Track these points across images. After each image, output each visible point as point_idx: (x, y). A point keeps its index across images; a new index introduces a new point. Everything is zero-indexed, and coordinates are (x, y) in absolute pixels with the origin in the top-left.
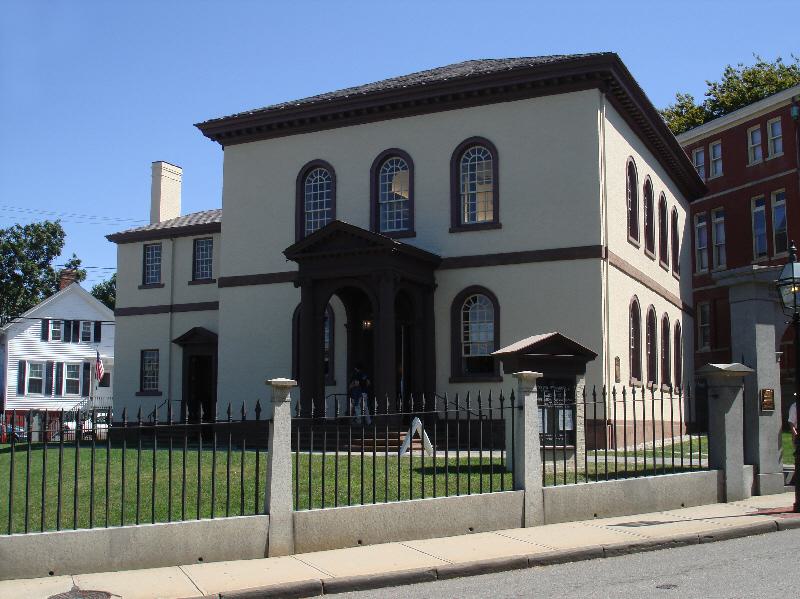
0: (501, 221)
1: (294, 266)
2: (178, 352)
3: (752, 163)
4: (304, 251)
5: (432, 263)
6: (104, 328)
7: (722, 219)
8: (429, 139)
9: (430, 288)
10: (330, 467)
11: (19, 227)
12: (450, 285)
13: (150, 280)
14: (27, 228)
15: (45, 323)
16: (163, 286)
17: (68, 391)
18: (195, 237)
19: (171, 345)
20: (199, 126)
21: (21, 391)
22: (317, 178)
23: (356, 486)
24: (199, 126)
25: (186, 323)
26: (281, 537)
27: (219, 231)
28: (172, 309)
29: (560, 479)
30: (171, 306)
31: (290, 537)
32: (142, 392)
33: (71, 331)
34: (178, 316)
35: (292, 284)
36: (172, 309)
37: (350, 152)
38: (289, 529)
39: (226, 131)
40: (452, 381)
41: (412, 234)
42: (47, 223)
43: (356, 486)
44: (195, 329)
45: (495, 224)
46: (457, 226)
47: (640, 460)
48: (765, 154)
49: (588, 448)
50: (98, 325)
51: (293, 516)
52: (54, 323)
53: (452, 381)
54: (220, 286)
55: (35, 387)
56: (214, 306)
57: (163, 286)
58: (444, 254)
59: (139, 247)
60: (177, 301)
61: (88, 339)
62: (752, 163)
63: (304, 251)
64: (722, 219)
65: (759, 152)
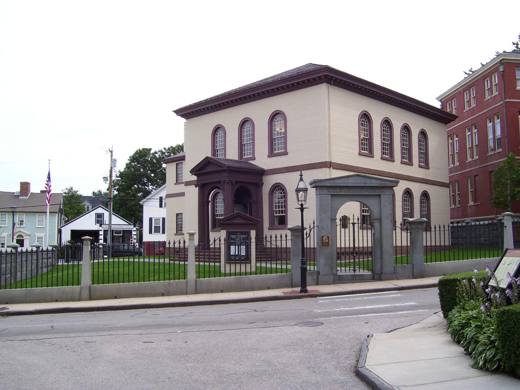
1: (195, 178)
4: (197, 171)
5: (261, 173)
8: (259, 111)
9: (259, 185)
10: (177, 268)
11: (165, 149)
12: (270, 181)
14: (169, 149)
17: (155, 232)
18: (177, 162)
20: (175, 112)
21: (150, 232)
24: (175, 112)
26: (85, 294)
27: (184, 159)
29: (212, 273)
31: (88, 294)
32: (177, 234)
38: (88, 291)
39: (188, 113)
40: (270, 229)
41: (254, 159)
47: (284, 267)
49: (256, 261)
51: (90, 287)
53: (270, 229)
54: (185, 185)
55: (157, 230)
56: (182, 194)
58: (266, 168)
63: (197, 171)
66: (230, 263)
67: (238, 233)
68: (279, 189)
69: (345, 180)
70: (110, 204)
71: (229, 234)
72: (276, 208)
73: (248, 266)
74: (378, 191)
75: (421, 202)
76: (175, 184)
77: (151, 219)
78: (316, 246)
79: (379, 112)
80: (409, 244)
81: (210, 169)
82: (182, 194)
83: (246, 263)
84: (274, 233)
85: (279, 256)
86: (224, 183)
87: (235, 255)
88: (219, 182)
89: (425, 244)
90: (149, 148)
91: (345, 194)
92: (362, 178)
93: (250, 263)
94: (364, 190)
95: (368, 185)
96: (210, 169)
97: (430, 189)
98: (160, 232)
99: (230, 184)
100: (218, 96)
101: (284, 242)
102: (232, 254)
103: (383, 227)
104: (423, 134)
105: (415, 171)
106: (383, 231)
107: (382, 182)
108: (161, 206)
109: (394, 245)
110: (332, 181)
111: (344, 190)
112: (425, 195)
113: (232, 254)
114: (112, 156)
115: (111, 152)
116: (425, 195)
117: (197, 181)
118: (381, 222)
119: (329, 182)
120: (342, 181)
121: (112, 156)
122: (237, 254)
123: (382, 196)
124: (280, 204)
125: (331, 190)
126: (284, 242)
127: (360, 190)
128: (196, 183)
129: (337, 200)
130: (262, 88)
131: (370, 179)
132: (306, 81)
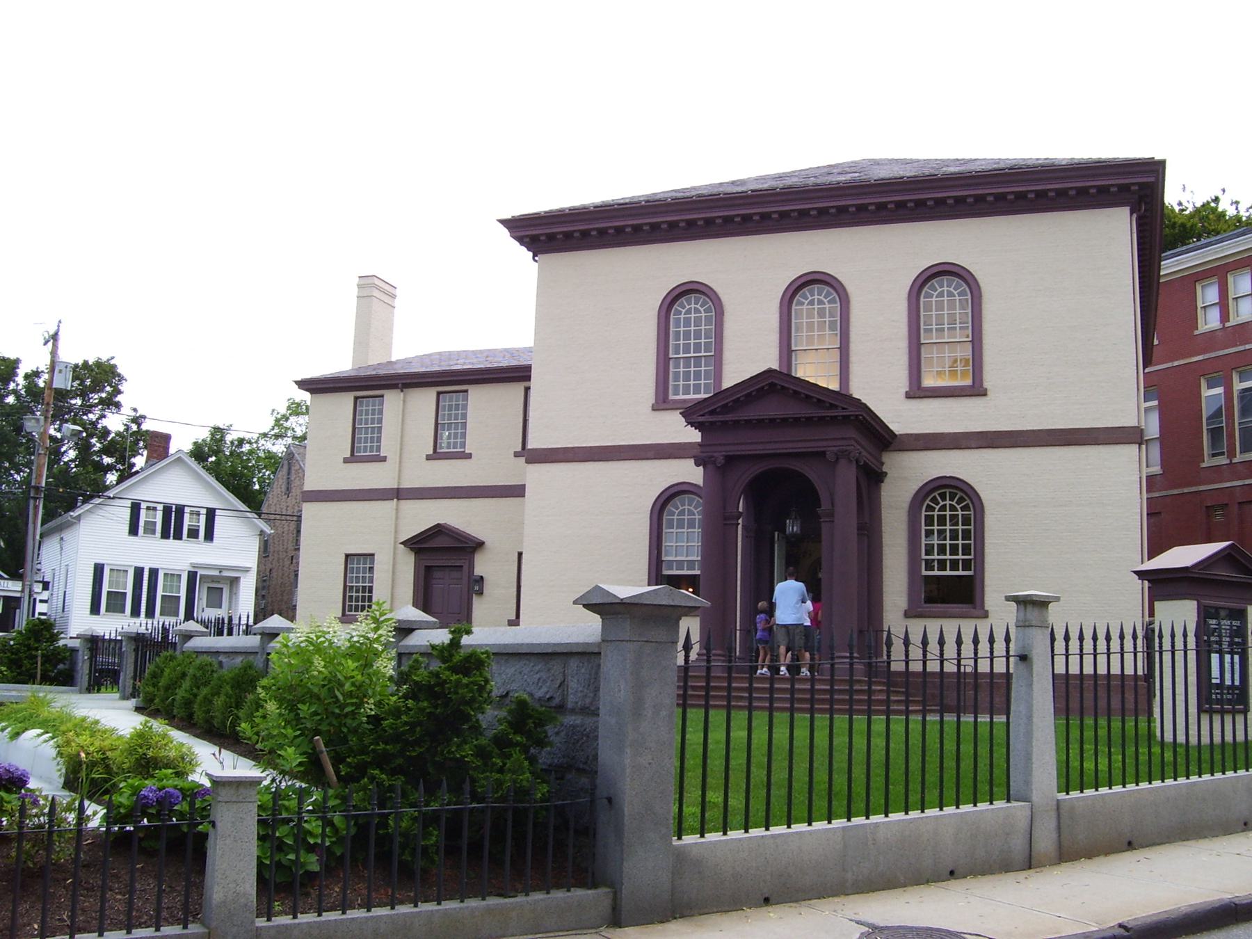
0: (986, 385)
1: (694, 436)
2: (407, 564)
3: (1202, 328)
6: (219, 521)
7: (1155, 403)
8: (877, 264)
9: (873, 477)
12: (908, 474)
13: (363, 450)
15: (135, 508)
16: (384, 459)
19: (395, 548)
20: (503, 222)
21: (95, 609)
22: (691, 308)
23: (736, 802)
25: (421, 517)
28: (399, 494)
30: (398, 489)
33: (173, 522)
34: (409, 506)
35: (692, 461)
36: (399, 494)
37: (753, 274)
39: (545, 234)
42: (86, 363)
43: (736, 802)
44: (438, 525)
45: (976, 390)
46: (917, 391)
48: (1225, 317)
50: (211, 514)
52: (192, 513)
56: (517, 491)
57: (384, 459)
59: (345, 402)
60: (406, 484)
61: (154, 532)
62: (1202, 328)
63: (712, 413)
64: (1155, 403)
65: (1214, 315)
66: (1211, 712)
70: (36, 507)
71: (1205, 614)
76: (346, 461)
77: (99, 570)
78: (1140, 672)
82: (517, 491)
83: (1234, 713)
84: (916, 628)
85: (951, 698)
87: (1220, 686)
90: (13, 357)
98: (123, 612)
100: (584, 207)
101: (1074, 660)
102: (1214, 681)
108: (133, 530)
113: (1214, 681)
117: (698, 444)
126: (1074, 660)
128: (697, 451)
130: (690, 210)
132: (543, 238)
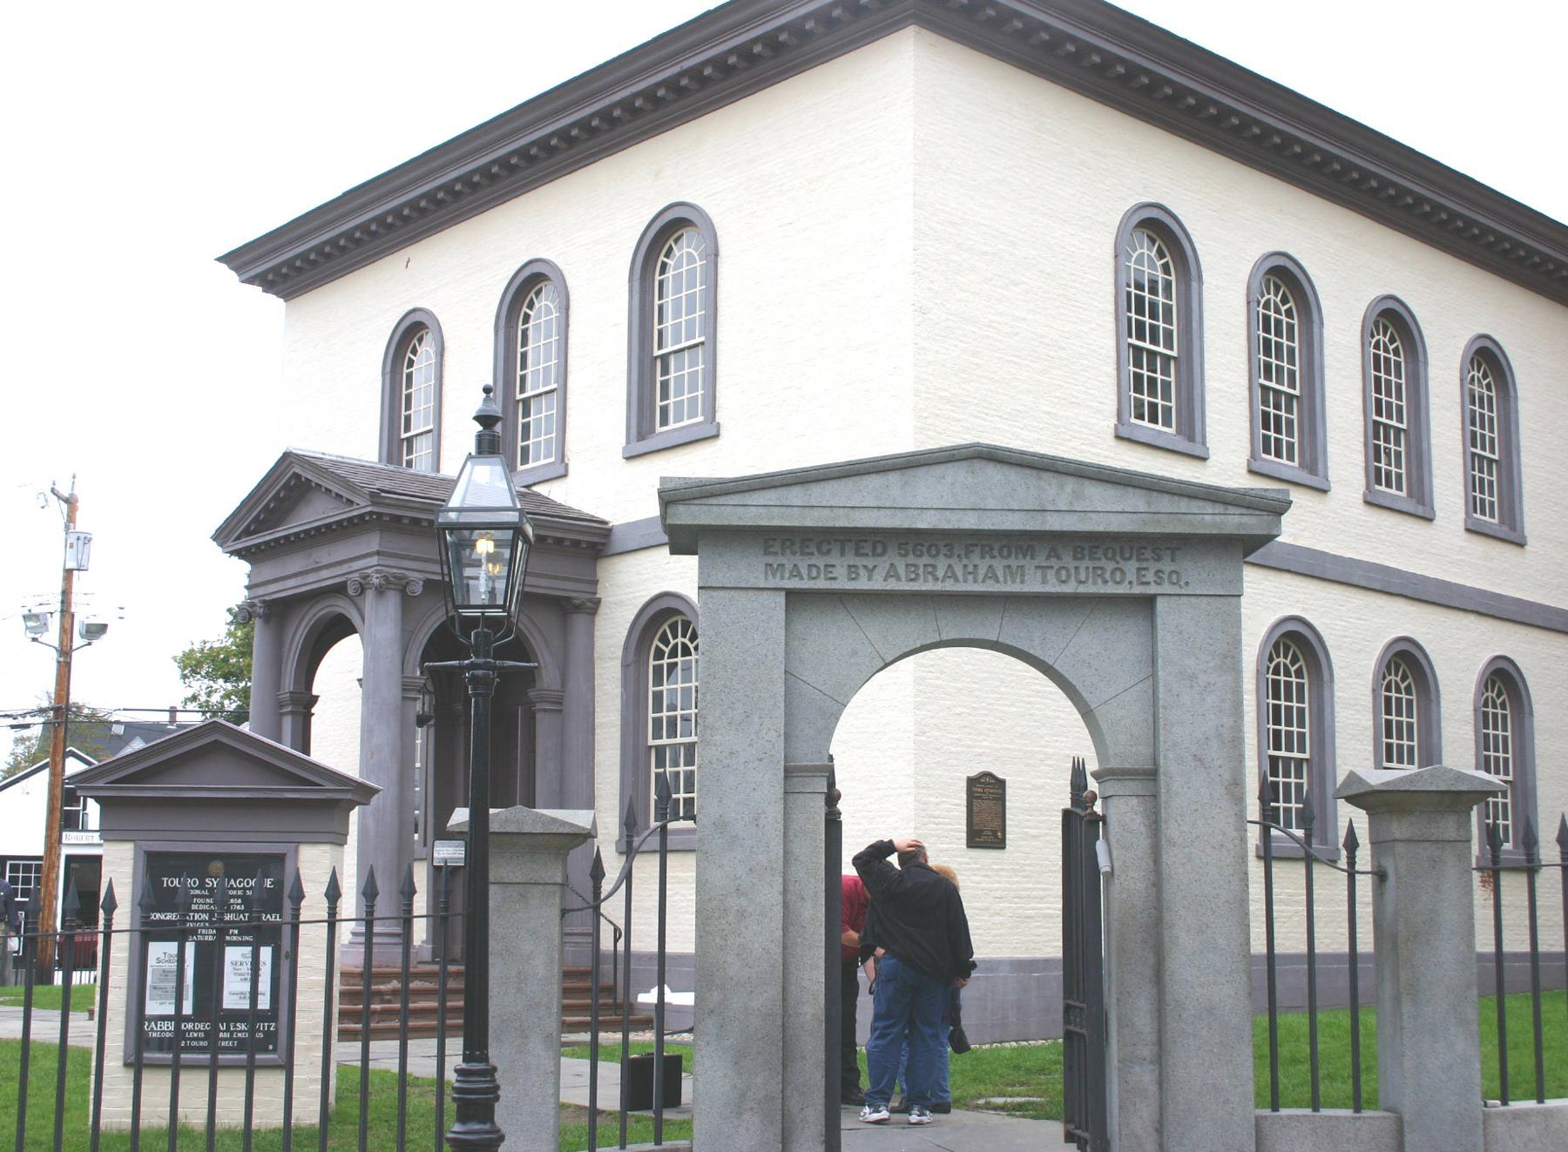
4: (248, 532)
39: (296, 261)
67: (217, 866)
68: (673, 628)
69: (892, 488)
72: (657, 736)
73: (269, 1086)
74: (1131, 567)
75: (1483, 720)
79: (1239, 221)
80: (1366, 944)
81: (315, 513)
86: (362, 589)
88: (339, 589)
89: (1484, 943)
91: (892, 585)
92: (1013, 474)
93: (288, 1067)
94: (1029, 564)
95: (1054, 523)
96: (315, 513)
97: (1529, 651)
99: (392, 602)
103: (1171, 830)
104: (1487, 359)
105: (1443, 548)
106: (1170, 858)
107: (1165, 504)
109: (1258, 946)
110: (796, 495)
111: (883, 564)
112: (1503, 681)
114: (71, 519)
115: (71, 502)
116: (1503, 681)
118: (1155, 796)
119: (770, 497)
120: (867, 491)
121: (71, 519)
122: (264, 1003)
123: (1161, 604)
124: (665, 714)
125: (788, 561)
127: (999, 565)
129: (832, 637)
131: (1071, 484)
